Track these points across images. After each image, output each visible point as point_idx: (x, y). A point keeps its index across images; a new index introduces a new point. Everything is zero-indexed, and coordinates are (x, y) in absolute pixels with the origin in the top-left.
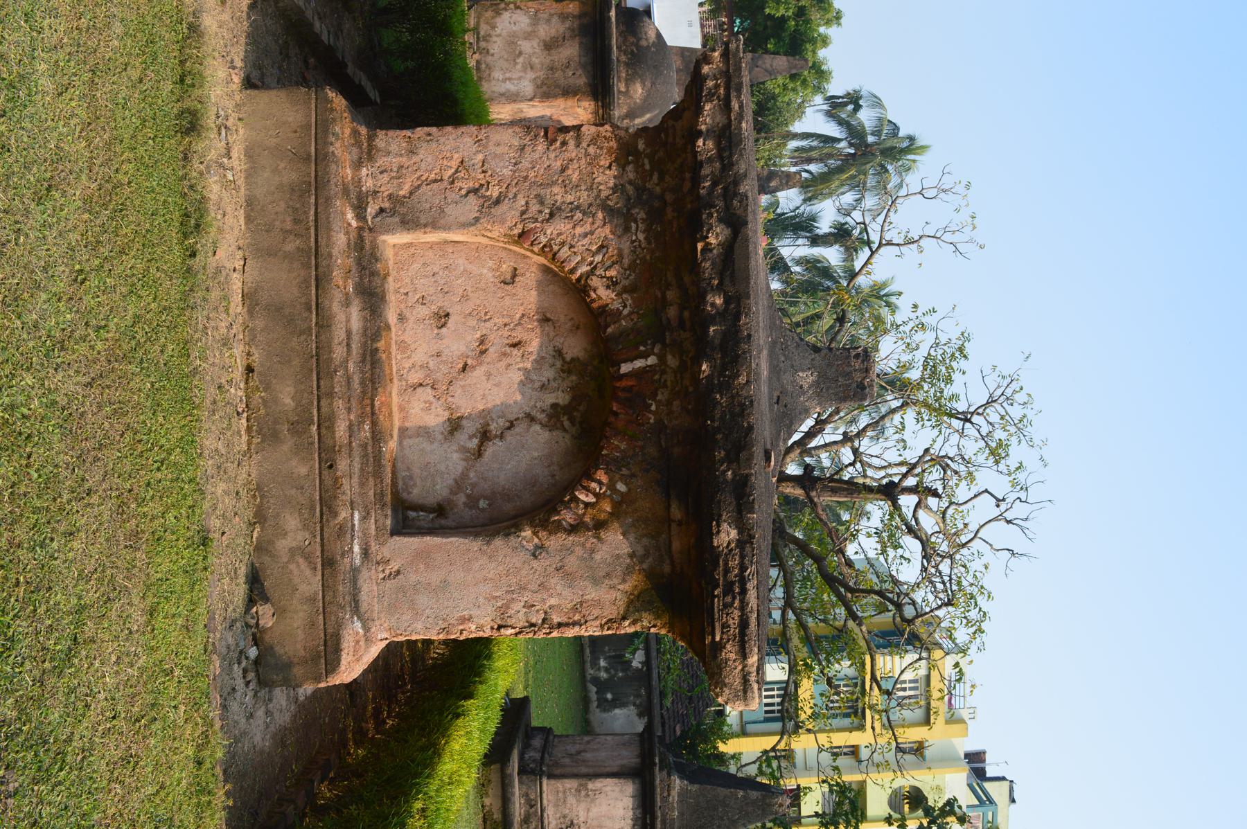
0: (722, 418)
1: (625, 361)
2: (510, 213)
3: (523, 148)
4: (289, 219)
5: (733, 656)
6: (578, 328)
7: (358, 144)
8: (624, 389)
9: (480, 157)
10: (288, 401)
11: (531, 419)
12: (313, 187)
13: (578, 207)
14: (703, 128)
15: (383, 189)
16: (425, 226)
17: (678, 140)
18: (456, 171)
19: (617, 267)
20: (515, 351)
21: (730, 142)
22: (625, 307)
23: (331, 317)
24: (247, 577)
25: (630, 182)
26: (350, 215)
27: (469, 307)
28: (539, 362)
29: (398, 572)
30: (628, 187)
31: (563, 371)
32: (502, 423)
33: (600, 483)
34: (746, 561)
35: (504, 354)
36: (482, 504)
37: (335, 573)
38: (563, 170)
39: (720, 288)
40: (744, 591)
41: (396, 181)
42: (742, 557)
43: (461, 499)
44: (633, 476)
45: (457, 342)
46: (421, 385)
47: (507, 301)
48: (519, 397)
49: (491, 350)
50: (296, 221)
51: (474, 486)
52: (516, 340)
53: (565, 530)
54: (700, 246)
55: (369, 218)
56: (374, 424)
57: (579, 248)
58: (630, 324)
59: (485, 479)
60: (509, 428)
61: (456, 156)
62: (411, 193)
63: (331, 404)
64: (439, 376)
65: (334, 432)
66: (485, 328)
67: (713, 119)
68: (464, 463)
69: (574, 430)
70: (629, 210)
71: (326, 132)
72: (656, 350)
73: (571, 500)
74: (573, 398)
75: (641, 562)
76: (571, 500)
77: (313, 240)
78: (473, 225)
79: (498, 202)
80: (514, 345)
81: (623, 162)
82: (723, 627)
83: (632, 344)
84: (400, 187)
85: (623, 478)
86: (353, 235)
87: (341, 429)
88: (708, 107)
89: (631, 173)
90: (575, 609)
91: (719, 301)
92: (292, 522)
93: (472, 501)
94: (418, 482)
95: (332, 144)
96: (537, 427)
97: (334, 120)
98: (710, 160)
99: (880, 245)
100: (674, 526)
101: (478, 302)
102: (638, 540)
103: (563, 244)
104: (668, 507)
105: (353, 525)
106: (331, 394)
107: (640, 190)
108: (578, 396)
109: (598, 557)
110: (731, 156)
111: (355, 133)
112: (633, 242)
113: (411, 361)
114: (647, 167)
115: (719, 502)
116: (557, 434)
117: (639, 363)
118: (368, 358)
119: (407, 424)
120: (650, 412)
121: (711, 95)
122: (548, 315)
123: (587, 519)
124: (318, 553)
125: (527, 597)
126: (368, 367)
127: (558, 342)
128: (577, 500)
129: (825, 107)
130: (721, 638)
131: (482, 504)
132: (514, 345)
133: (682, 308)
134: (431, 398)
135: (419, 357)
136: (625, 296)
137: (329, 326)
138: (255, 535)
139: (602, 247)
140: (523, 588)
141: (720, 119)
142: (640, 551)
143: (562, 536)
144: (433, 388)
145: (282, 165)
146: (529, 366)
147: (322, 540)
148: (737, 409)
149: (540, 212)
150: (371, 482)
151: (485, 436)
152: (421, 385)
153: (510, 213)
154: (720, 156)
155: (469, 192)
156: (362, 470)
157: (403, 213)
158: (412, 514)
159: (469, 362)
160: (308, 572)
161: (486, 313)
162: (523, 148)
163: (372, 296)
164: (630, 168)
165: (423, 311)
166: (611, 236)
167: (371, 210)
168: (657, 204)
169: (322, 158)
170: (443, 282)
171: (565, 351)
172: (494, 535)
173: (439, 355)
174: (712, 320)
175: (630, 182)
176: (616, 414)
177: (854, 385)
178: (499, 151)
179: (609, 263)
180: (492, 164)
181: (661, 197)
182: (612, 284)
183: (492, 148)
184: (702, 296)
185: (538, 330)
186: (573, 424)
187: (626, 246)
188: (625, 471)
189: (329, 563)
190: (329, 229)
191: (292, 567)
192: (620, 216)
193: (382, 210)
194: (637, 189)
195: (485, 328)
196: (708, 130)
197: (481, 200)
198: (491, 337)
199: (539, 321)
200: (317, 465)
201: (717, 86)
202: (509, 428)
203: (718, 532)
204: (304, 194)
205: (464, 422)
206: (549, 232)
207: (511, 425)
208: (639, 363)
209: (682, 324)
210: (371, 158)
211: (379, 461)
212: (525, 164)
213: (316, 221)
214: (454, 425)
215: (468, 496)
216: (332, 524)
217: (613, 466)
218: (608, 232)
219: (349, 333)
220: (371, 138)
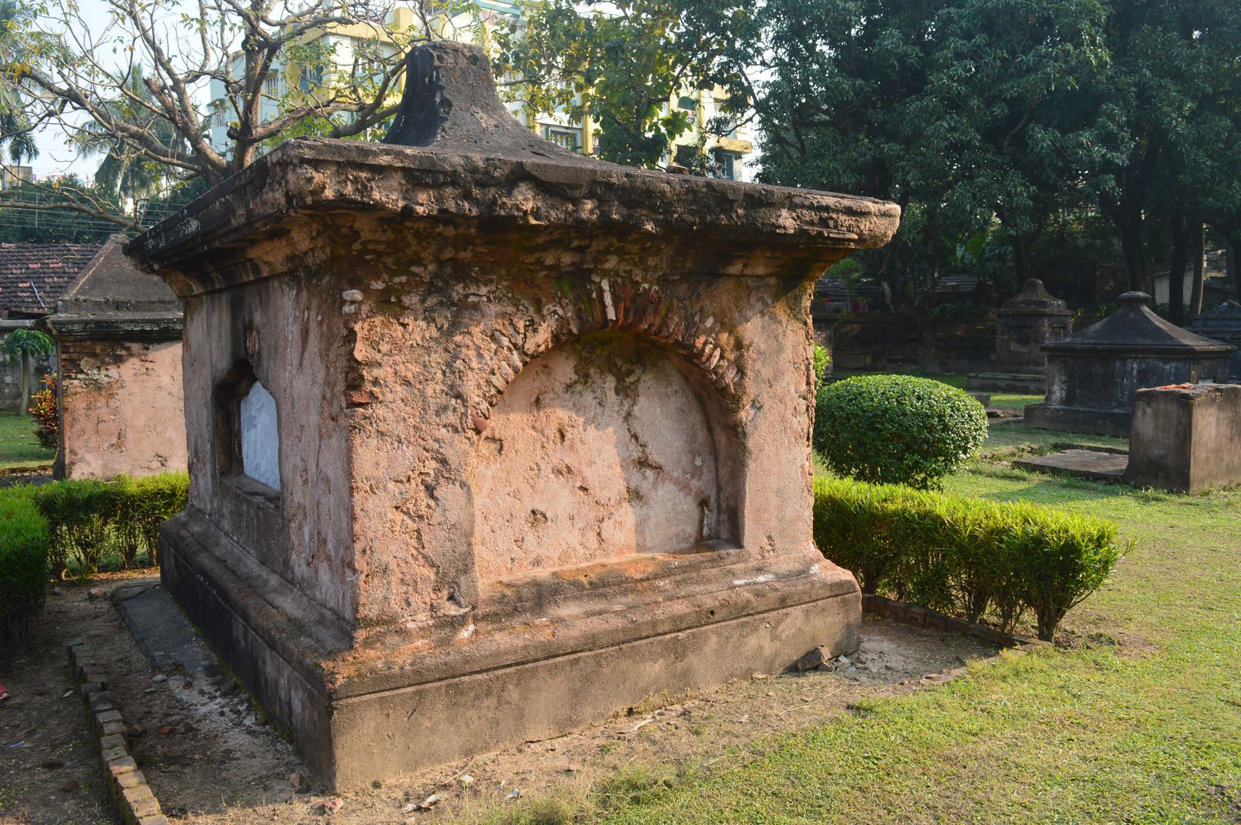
0: (693, 213)
1: (605, 314)
2: (456, 446)
3: (381, 434)
4: (486, 703)
6: (546, 367)
7: (379, 638)
8: (625, 317)
9: (391, 485)
10: (657, 667)
11: (628, 416)
12: (448, 681)
13: (449, 365)
14: (401, 204)
15: (428, 601)
16: (470, 545)
17: (384, 239)
18: (407, 513)
19: (515, 320)
20: (568, 435)
21: (431, 171)
22: (555, 312)
23: (585, 636)
24: (988, 656)
25: (423, 301)
26: (465, 633)
27: (525, 488)
28: (578, 408)
29: (769, 538)
30: (429, 303)
31: (586, 382)
32: (632, 447)
33: (705, 343)
34: (807, 203)
35: (571, 447)
36: (698, 462)
37: (790, 596)
38: (407, 383)
39: (576, 202)
40: (827, 209)
41: (420, 585)
42: (803, 206)
43: (695, 483)
44: (702, 310)
45: (559, 499)
46: (599, 534)
47: (520, 446)
48: (611, 429)
49: (567, 461)
50: (488, 693)
51: (685, 472)
52: (558, 435)
53: (742, 378)
54: (533, 222)
55: (462, 611)
56: (656, 577)
57: (494, 364)
58: (571, 307)
59: (680, 461)
60: (637, 439)
61: (390, 516)
62: (433, 565)
63: (662, 622)
64: (591, 516)
65: (685, 615)
66: (546, 469)
67: (392, 190)
68: (666, 483)
69: (638, 371)
70: (453, 304)
71: (387, 678)
72: (597, 280)
73: (716, 373)
74: (611, 371)
75: (767, 305)
76: (716, 373)
77: (508, 670)
78: (469, 489)
79: (444, 462)
80: (563, 436)
81: (398, 309)
82: (849, 231)
83: (588, 302)
84: (425, 580)
85: (702, 321)
86: (483, 626)
87: (680, 608)
88: (376, 195)
89: (411, 300)
90: (797, 369)
91: (589, 205)
92: (752, 642)
93: (696, 472)
94: (681, 528)
95: (402, 668)
96: (636, 408)
97: (372, 671)
98: (439, 200)
100: (746, 272)
101: (521, 479)
102: (752, 307)
103: (489, 382)
104: (730, 275)
105: (746, 584)
106: (654, 624)
107: (431, 288)
108: (610, 367)
109: (763, 347)
110: (445, 173)
111: (367, 643)
112: (489, 300)
113: (578, 547)
114: (404, 279)
115: (763, 224)
116: (642, 388)
117: (608, 299)
118: (601, 591)
119: (634, 545)
120: (650, 289)
121: (364, 189)
122: (533, 399)
123: (732, 357)
124: (775, 613)
125: (789, 414)
126: (608, 590)
127: (559, 388)
128: (717, 366)
131: (698, 462)
132: (563, 436)
133: (567, 248)
134: (612, 521)
135: (573, 538)
136: (545, 312)
137: (593, 636)
138: (760, 676)
139: (492, 337)
140: (783, 419)
141: (396, 180)
142: (759, 306)
143: (748, 382)
144: (602, 521)
145: (427, 723)
146: (582, 420)
147: (766, 611)
148: (690, 197)
149: (455, 410)
150: (704, 572)
151: (643, 463)
152: (599, 534)
153: (456, 446)
154: (437, 186)
155: (432, 496)
156: (697, 583)
157: (453, 575)
158: (705, 531)
159: (578, 484)
160: (788, 621)
161: (531, 469)
162: (381, 434)
163: (541, 596)
164: (406, 300)
165: (530, 538)
166: (482, 326)
167: (452, 610)
168: (448, 270)
169: (419, 677)
170: (500, 520)
171: (568, 381)
172: (743, 447)
173: (572, 518)
174: (605, 216)
175: (423, 301)
176: (651, 325)
177: (474, 67)
178: (384, 463)
179: (511, 330)
180: (401, 471)
181: (441, 263)
182: (532, 326)
183: (380, 473)
184: (580, 222)
185: (548, 411)
186: (632, 372)
187: (493, 309)
188: (697, 319)
189: (784, 602)
190: (497, 654)
191: (784, 636)
192: (461, 312)
193: (451, 598)
194: (430, 293)
195: (546, 469)
196: (404, 198)
197: (442, 480)
198: (555, 461)
199: (539, 410)
200: (710, 627)
201: (356, 180)
202: (637, 439)
203: (785, 228)
204: (459, 690)
205: (632, 486)
206: (477, 399)
207: (635, 437)
208: (608, 299)
209: (580, 250)
210: (392, 620)
211: (686, 567)
212: (400, 430)
213: (488, 670)
214: (635, 495)
215: (693, 476)
217: (692, 329)
218: (477, 330)
219: (589, 614)
220: (369, 623)
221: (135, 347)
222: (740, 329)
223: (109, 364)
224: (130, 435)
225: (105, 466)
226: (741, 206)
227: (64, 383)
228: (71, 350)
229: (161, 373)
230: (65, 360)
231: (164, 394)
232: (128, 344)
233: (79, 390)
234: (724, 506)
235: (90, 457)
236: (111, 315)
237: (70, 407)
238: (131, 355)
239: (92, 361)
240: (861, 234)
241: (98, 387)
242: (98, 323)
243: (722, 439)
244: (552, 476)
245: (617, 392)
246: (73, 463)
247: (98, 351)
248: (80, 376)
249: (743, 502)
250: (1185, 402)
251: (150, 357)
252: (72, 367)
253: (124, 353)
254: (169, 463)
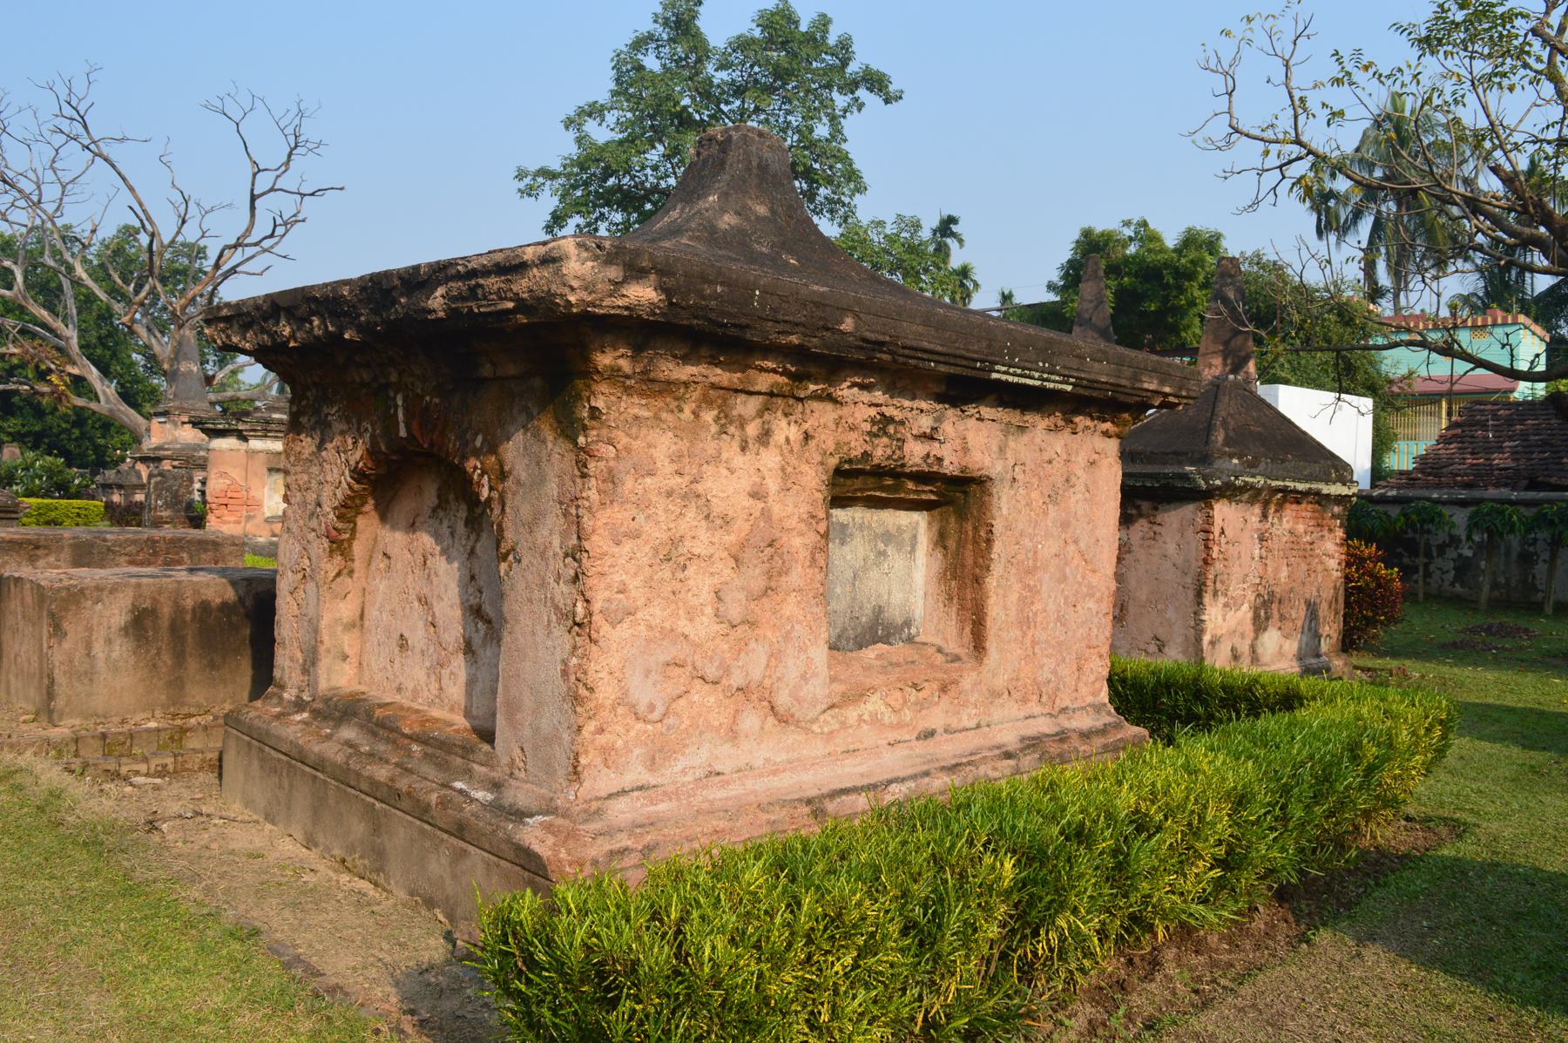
5: (524, 282)
82: (501, 299)
99: (1298, 142)
129: (1333, 238)
130: (511, 300)
142: (522, 418)
147: (441, 829)
216: (434, 813)
222: (501, 449)
224: (1132, 609)
226: (402, 295)
231: (1168, 564)
232: (1139, 502)
238: (1141, 515)
240: (517, 298)
244: (416, 604)
245: (466, 524)
251: (1159, 519)
253: (1134, 512)
254: (1166, 650)
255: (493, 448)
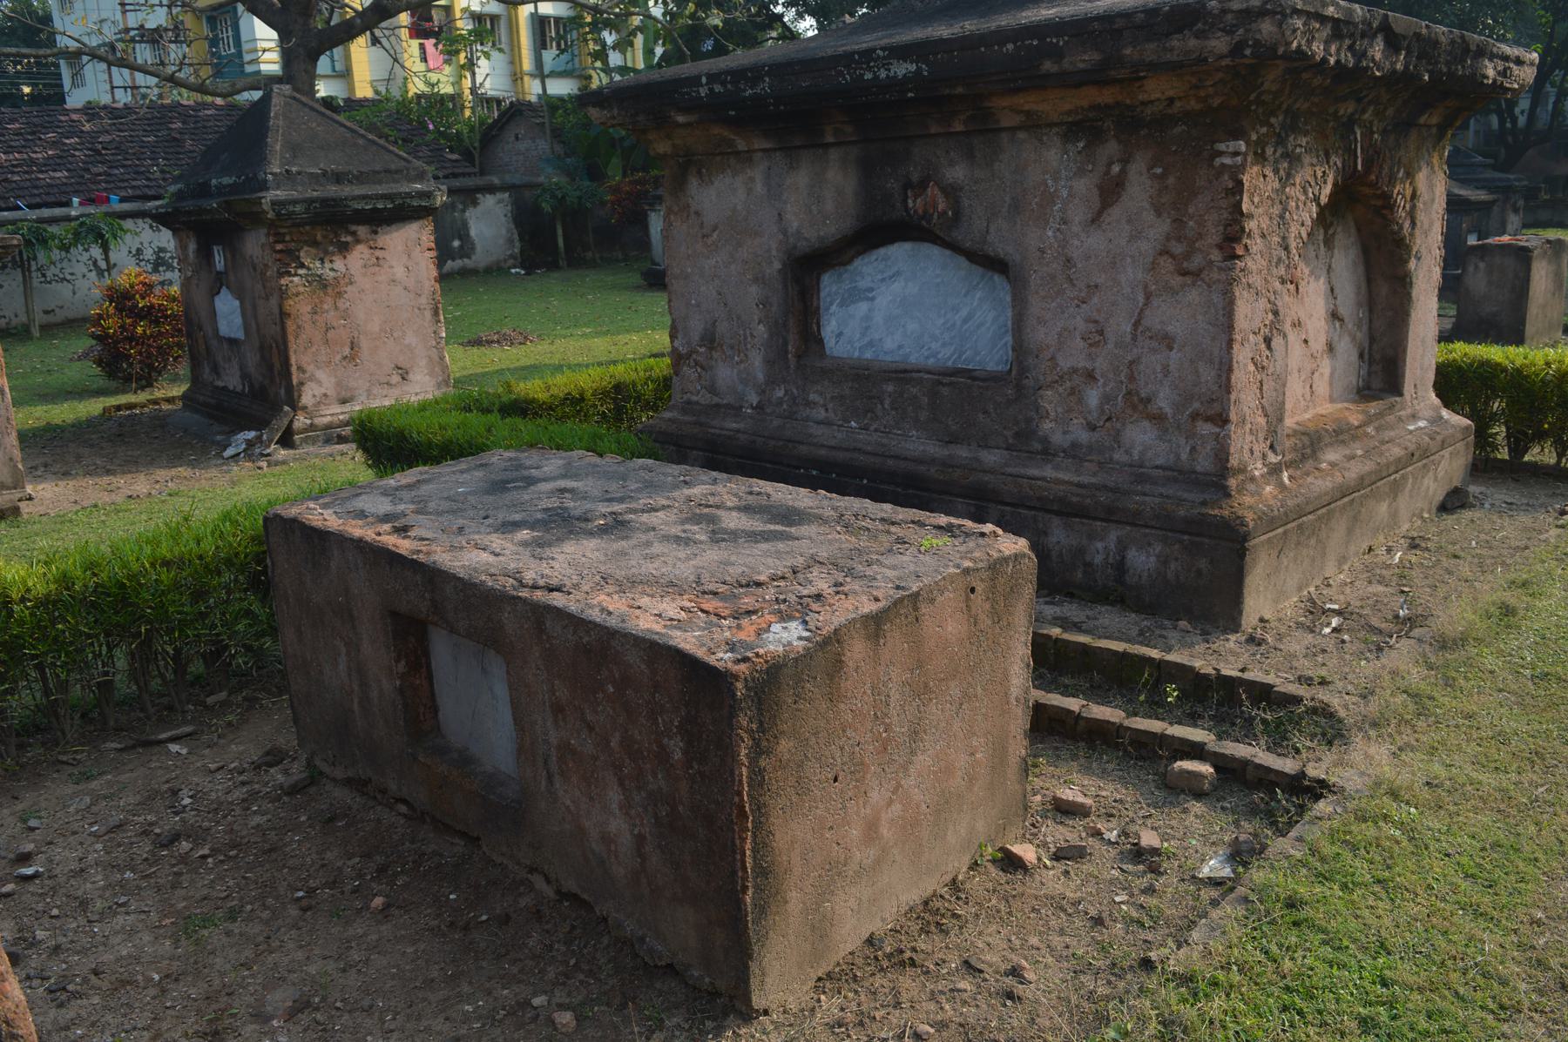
143: (1417, 232)
221: (362, 231)
223: (333, 254)
224: (365, 344)
225: (339, 384)
227: (283, 282)
228: (288, 238)
229: (394, 263)
230: (281, 251)
232: (354, 228)
233: (301, 289)
234: (1377, 357)
235: (321, 375)
236: (333, 190)
237: (293, 312)
238: (358, 241)
239: (313, 251)
241: (322, 283)
242: (324, 201)
243: (1383, 290)
246: (302, 384)
247: (319, 237)
248: (301, 272)
249: (1405, 351)
250: (1523, 256)
252: (288, 260)
253: (349, 239)
254: (411, 376)
255: (1410, 175)
